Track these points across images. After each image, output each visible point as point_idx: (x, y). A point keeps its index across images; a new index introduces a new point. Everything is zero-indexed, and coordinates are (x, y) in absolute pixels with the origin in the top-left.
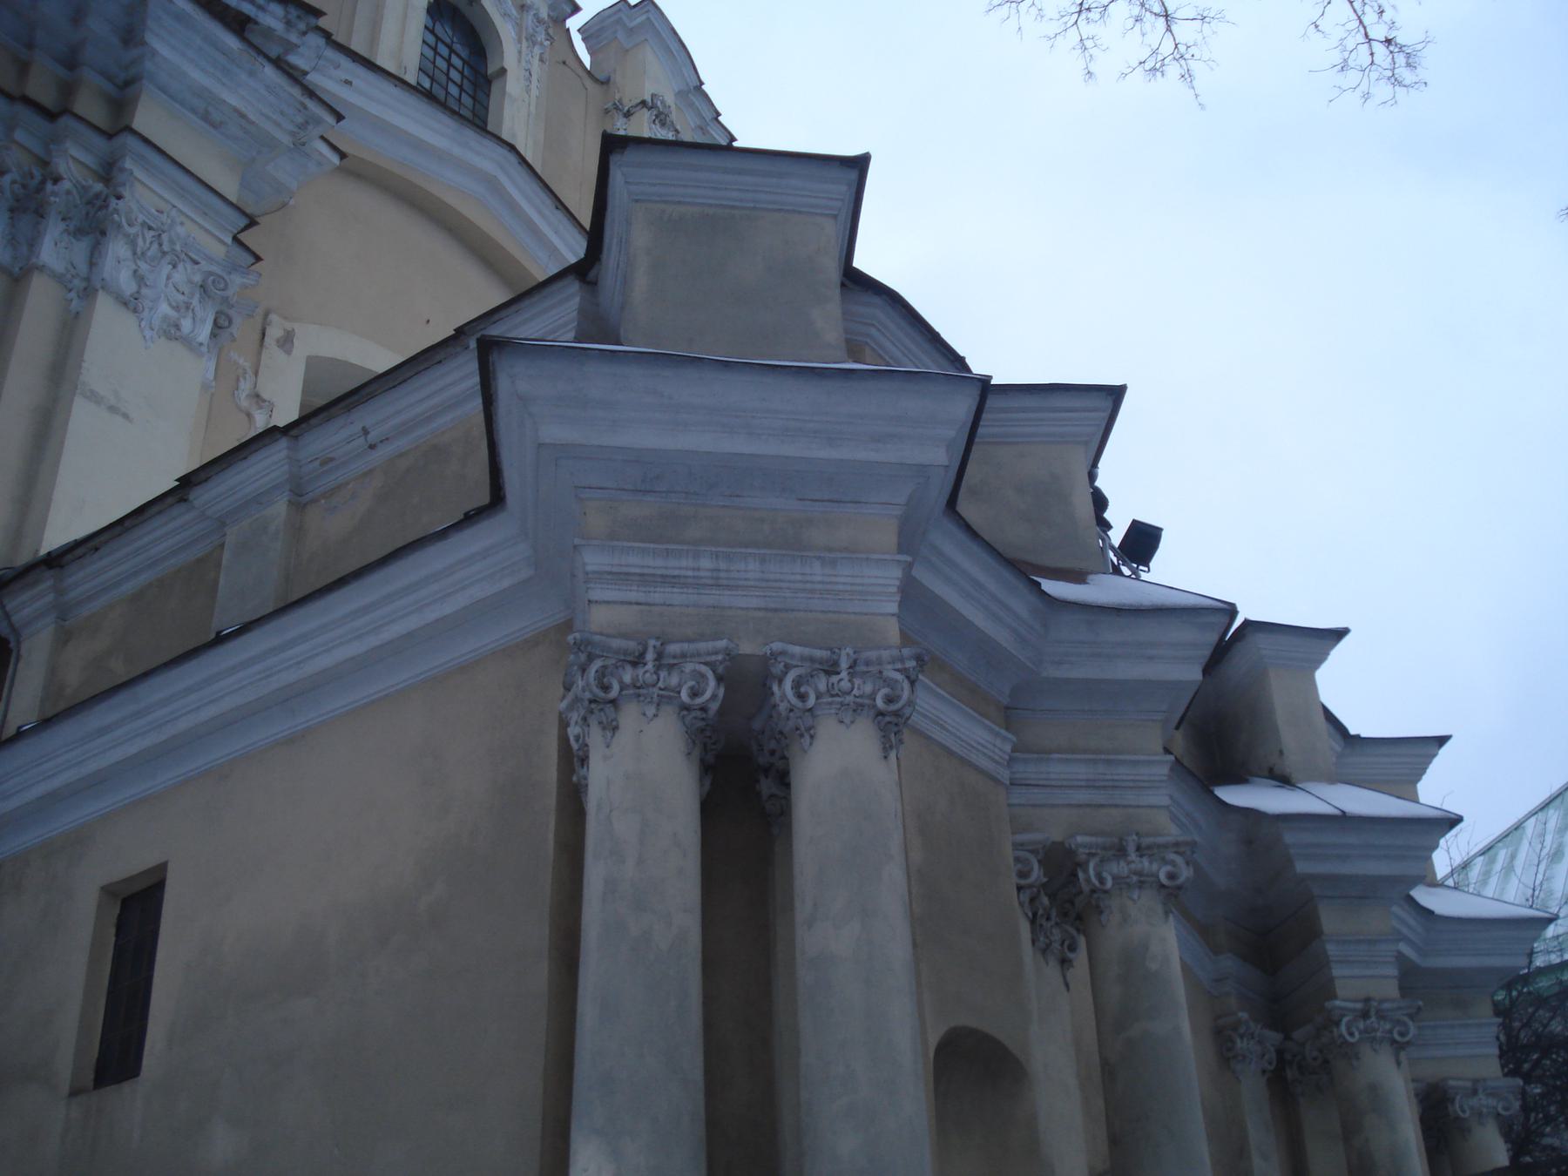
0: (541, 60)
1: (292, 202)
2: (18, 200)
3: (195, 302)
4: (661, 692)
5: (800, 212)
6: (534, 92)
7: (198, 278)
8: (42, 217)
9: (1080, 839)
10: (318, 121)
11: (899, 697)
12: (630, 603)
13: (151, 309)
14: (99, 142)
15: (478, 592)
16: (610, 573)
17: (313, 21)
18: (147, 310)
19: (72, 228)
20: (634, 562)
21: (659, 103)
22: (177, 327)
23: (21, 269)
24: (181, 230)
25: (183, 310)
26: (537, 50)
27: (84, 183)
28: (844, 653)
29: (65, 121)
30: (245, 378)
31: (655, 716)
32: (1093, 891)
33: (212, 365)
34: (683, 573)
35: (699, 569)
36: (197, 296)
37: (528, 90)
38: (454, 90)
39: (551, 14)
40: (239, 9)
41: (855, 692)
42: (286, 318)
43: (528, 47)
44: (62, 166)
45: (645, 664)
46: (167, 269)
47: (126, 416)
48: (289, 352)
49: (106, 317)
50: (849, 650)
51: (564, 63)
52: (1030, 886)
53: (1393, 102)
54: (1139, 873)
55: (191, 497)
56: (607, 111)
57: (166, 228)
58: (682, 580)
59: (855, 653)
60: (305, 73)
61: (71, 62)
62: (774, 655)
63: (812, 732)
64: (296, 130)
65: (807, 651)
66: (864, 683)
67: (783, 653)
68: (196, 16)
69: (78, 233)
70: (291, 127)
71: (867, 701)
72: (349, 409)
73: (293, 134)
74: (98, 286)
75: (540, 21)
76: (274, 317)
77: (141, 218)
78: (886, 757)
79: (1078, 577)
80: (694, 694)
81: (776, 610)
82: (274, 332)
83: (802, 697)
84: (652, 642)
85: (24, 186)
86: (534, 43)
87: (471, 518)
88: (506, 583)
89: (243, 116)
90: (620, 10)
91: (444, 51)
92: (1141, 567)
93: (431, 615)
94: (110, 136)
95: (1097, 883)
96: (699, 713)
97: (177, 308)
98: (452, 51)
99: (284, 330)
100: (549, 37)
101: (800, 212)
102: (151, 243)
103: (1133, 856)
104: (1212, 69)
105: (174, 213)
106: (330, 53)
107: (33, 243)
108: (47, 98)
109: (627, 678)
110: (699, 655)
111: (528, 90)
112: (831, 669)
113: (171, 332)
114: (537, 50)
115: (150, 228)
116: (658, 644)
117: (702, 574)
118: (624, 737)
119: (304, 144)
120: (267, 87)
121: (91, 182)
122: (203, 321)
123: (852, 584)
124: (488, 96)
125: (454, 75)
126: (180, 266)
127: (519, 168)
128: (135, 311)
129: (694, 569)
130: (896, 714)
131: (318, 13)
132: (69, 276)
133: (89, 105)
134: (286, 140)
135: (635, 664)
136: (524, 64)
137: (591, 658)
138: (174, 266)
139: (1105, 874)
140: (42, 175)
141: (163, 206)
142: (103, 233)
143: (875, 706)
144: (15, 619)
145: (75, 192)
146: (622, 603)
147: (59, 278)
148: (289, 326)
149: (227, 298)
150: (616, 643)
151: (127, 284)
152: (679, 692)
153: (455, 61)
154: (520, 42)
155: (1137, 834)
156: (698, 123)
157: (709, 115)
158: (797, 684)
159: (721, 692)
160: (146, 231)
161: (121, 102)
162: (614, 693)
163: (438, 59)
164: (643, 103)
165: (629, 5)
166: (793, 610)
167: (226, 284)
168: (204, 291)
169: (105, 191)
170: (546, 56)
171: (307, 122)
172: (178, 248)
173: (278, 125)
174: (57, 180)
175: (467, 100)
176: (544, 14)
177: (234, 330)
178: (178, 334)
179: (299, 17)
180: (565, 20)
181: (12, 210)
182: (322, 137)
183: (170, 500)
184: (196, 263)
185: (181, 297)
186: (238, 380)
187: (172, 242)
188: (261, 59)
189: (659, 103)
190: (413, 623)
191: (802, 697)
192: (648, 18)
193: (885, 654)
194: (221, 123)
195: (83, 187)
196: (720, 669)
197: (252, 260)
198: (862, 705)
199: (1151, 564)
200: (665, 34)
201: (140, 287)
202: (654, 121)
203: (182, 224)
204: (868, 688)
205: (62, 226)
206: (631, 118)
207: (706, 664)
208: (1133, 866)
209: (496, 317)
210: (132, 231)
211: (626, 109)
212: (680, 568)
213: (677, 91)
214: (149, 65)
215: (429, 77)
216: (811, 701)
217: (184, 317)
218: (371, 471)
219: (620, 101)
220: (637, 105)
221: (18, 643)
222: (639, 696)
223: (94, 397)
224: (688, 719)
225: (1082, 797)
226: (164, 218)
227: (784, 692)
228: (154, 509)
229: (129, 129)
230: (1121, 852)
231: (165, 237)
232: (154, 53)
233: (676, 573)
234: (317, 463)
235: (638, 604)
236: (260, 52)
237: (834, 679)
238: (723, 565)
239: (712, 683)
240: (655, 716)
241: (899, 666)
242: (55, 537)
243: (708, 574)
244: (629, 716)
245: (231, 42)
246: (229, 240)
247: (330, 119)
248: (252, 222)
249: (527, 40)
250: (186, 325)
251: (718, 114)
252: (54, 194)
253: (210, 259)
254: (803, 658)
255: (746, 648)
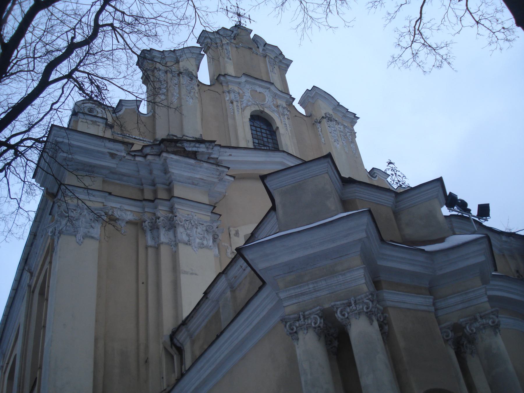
0: (288, 119)
1: (227, 194)
2: (151, 227)
3: (206, 235)
4: (307, 326)
5: (317, 175)
6: (289, 129)
7: (204, 229)
8: (159, 229)
9: (461, 320)
10: (223, 172)
11: (370, 307)
12: (294, 304)
13: (194, 243)
14: (167, 203)
15: (269, 307)
16: (288, 297)
17: (213, 144)
18: (193, 243)
19: (167, 229)
20: (292, 292)
21: (328, 115)
22: (203, 244)
23: (157, 245)
24: (196, 218)
25: (203, 239)
26: (286, 117)
27: (166, 216)
28: (351, 299)
29: (157, 201)
30: (228, 249)
31: (307, 333)
32: (471, 334)
33: (217, 250)
34: (306, 291)
35: (310, 288)
36: (206, 233)
37: (287, 129)
38: (265, 140)
39: (287, 104)
40: (192, 150)
41: (358, 309)
42: (235, 227)
43: (283, 117)
44: (159, 214)
45: (301, 320)
46: (195, 230)
47: (196, 274)
48: (238, 237)
49: (183, 251)
50: (353, 298)
51: (296, 116)
52: (451, 339)
53: (511, 47)
54: (483, 324)
55: (208, 297)
56: (314, 124)
57: (191, 219)
58: (307, 293)
59: (354, 298)
60: (217, 158)
61: (154, 184)
62: (333, 306)
63: (349, 324)
64: (218, 177)
65: (342, 302)
66: (359, 306)
67: (335, 305)
68: (180, 159)
69: (169, 229)
70: (216, 177)
71: (362, 311)
72: (235, 262)
73: (217, 178)
74: (178, 242)
75: (284, 108)
76: (231, 229)
77: (184, 219)
78: (371, 324)
79: (442, 240)
80: (315, 323)
81: (332, 293)
82: (233, 233)
83: (344, 315)
84: (301, 313)
85: (152, 223)
86: (284, 115)
87: (260, 288)
88: (274, 303)
89: (202, 179)
90: (307, 93)
91: (259, 130)
92: (487, 218)
93: (261, 316)
94: (169, 200)
95: (470, 332)
96: (318, 328)
97: (201, 239)
98: (261, 128)
99: (235, 231)
100: (289, 111)
101: (317, 175)
102: (189, 224)
103: (480, 320)
104: (454, 59)
105: (192, 213)
106: (222, 150)
107: (158, 237)
108: (151, 197)
109: (297, 325)
110: (314, 312)
111: (287, 129)
112: (349, 305)
113: (202, 246)
114: (286, 117)
115: (187, 220)
116: (302, 313)
117: (311, 289)
118: (301, 341)
119: (222, 179)
120: (206, 169)
121: (168, 215)
122: (209, 240)
123: (351, 278)
124: (276, 136)
125: (264, 135)
126: (199, 227)
127: (288, 156)
128: (190, 245)
129: (308, 289)
130: (371, 311)
131: (215, 141)
132: (170, 242)
133: (162, 194)
134: (216, 180)
135: (298, 320)
136: (283, 123)
137: (286, 322)
138: (197, 228)
139: (472, 328)
140: (155, 218)
141: (189, 213)
142: (175, 227)
143: (364, 311)
144: (180, 341)
145: (165, 219)
146: (292, 304)
147: (167, 244)
148: (236, 229)
149: (214, 231)
150: (292, 316)
151: (185, 238)
152: (312, 324)
153: (263, 131)
154: (280, 117)
155: (479, 313)
156: (342, 115)
157: (345, 111)
158: (341, 312)
159: (322, 321)
160: (186, 222)
161: (170, 190)
162: (295, 330)
163: (258, 133)
164: (323, 117)
165: (309, 90)
166: (337, 291)
167: (212, 227)
168: (207, 231)
169: (173, 215)
170: (290, 117)
171: (220, 173)
172: (196, 222)
173: (213, 177)
174: (159, 218)
175: (270, 141)
176: (285, 105)
177: (220, 238)
178: (203, 246)
179: (209, 145)
180: (292, 103)
181: (150, 230)
182: (227, 175)
183: (204, 299)
184: (203, 224)
185: (202, 235)
186: (226, 250)
187: (194, 222)
188: (202, 162)
189: (328, 115)
190: (258, 319)
191: (344, 315)
192: (316, 92)
193: (363, 296)
194: (198, 184)
195: (166, 217)
196: (320, 315)
197: (219, 216)
198: (360, 312)
199: (490, 215)
200: (323, 94)
201: (189, 238)
202: (328, 121)
203: (196, 216)
204: (361, 307)
205: (164, 229)
206: (321, 123)
207: (316, 314)
208: (480, 323)
209: (259, 227)
210: (182, 224)
211: (319, 121)
212: (305, 290)
213: (332, 108)
214: (173, 177)
215: (256, 139)
216: (346, 315)
217: (204, 241)
218: (246, 276)
219: (316, 119)
220: (321, 119)
221: (183, 347)
222: (301, 329)
223: (186, 273)
224: (316, 330)
225: (460, 306)
226: (190, 216)
227: (338, 315)
228: (202, 302)
229: (173, 197)
230: (476, 320)
231: (192, 221)
232: (173, 173)
233: (304, 291)
234: (233, 279)
235: (296, 303)
236: (201, 161)
237: (351, 307)
238: (315, 285)
239: (319, 319)
240: (307, 333)
241: (367, 298)
242: (186, 314)
243: (312, 289)
244: (301, 335)
245: (192, 161)
246: (210, 214)
247: (226, 170)
248: (215, 207)
249: (282, 115)
250: (205, 242)
251: (347, 110)
252: (159, 222)
253: (206, 222)
254: (341, 304)
255: (326, 306)
